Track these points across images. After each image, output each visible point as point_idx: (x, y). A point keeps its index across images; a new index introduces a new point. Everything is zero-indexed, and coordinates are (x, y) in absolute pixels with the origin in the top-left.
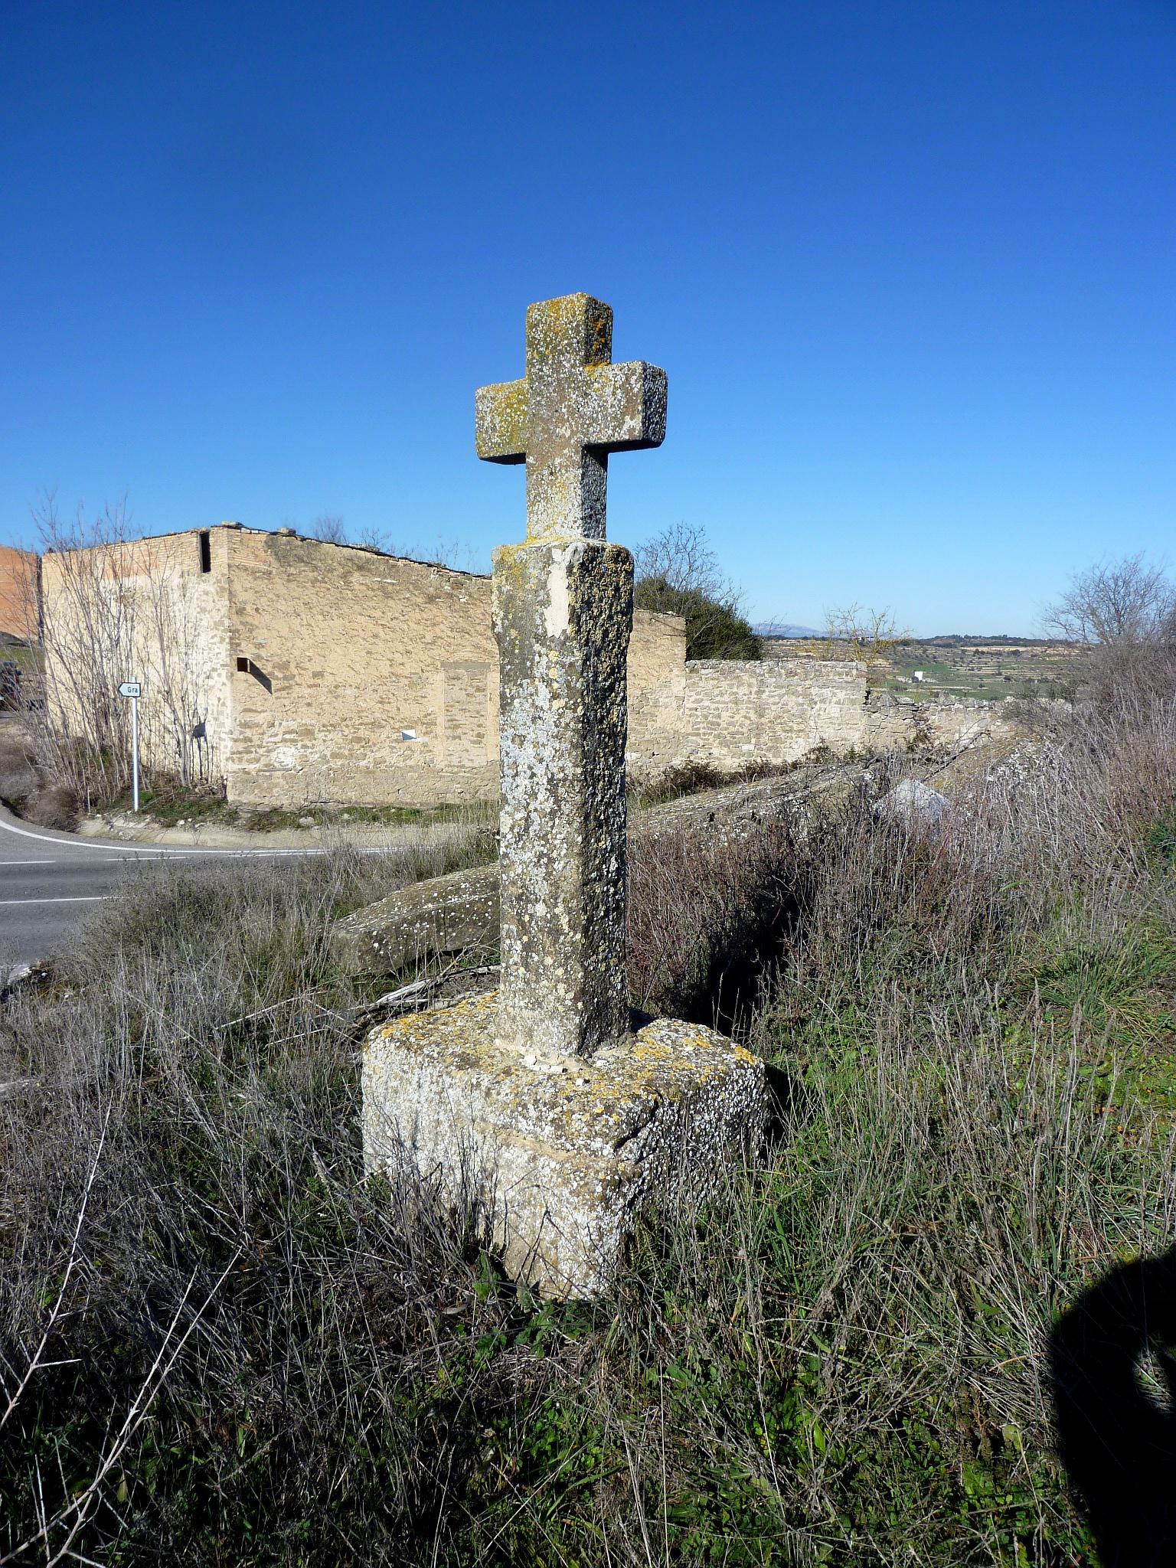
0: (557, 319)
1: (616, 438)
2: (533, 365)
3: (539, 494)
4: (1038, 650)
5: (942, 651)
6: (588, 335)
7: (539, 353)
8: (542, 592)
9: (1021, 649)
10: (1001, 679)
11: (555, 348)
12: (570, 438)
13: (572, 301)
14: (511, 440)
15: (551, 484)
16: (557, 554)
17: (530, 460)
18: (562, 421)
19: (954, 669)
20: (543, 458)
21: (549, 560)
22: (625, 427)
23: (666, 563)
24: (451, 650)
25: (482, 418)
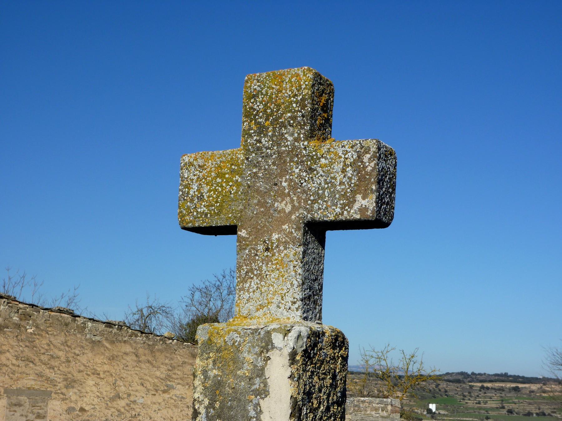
0: (280, 91)
1: (346, 216)
2: (250, 136)
3: (251, 270)
4: (534, 387)
5: (452, 386)
6: (314, 110)
7: (257, 123)
8: (257, 381)
9: (520, 386)
10: (504, 412)
11: (276, 120)
12: (290, 213)
13: (298, 75)
14: (220, 211)
15: (267, 260)
16: (277, 339)
17: (243, 233)
18: (282, 195)
19: (463, 402)
20: (258, 232)
21: (267, 345)
22: (356, 206)
23: (219, 303)
24: (15, 377)
25: (188, 186)
